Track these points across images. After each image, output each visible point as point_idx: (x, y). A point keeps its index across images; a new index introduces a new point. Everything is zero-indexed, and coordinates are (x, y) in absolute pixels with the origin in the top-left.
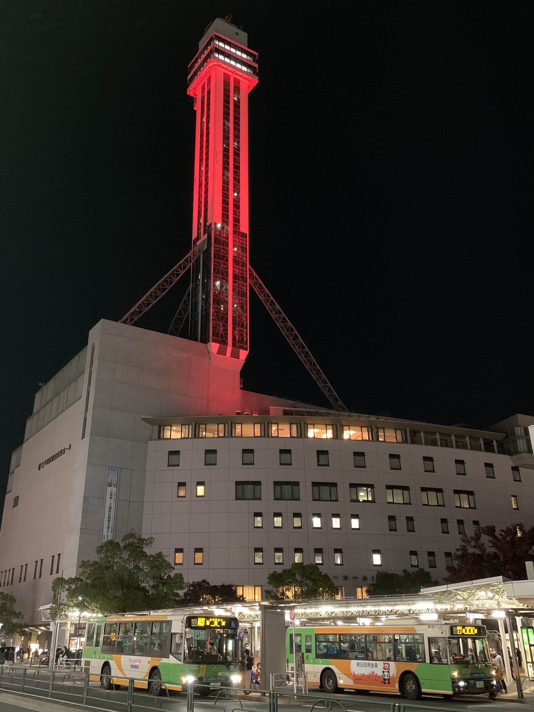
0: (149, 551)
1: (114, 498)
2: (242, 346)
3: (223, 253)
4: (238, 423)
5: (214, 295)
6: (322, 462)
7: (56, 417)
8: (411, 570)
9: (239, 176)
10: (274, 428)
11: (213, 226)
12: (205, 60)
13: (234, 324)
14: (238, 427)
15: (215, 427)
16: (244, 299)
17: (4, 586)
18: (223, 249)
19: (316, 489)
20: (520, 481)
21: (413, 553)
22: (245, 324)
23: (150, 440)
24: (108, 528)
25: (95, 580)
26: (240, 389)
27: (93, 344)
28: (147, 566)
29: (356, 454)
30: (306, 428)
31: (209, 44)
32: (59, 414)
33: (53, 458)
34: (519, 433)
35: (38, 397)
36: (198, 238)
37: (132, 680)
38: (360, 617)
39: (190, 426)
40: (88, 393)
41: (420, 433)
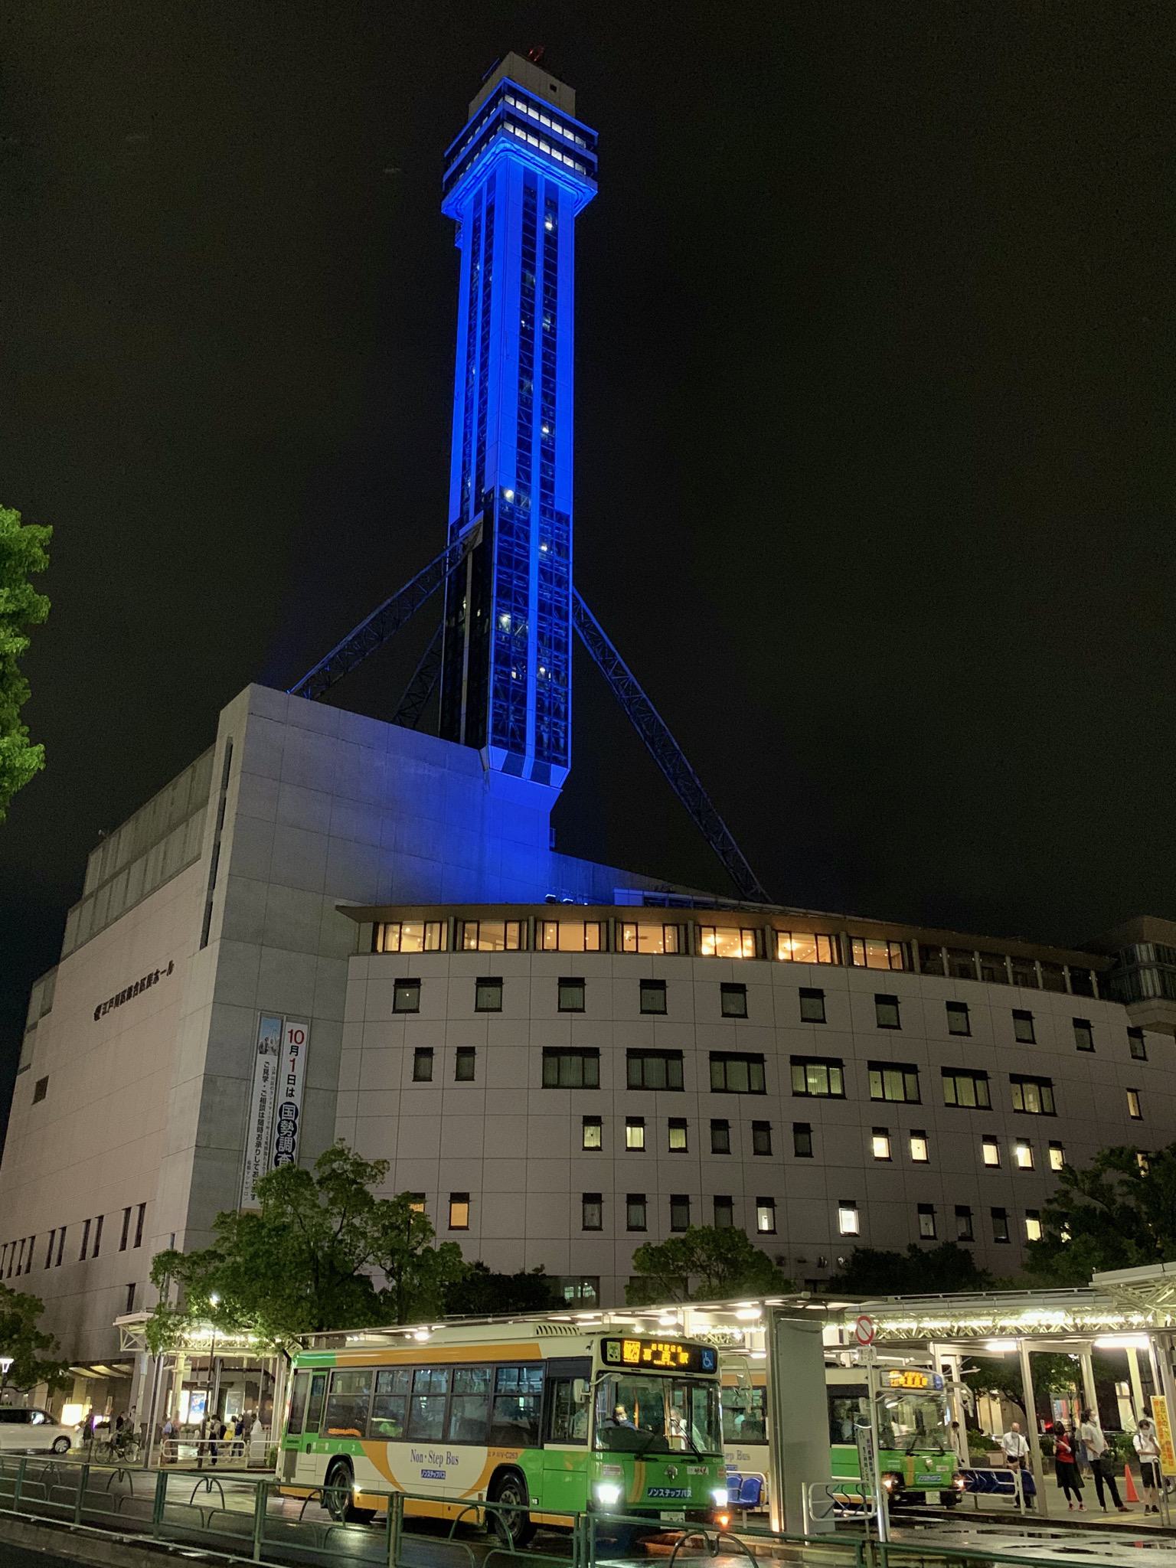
0: (381, 1191)
1: (273, 1078)
2: (555, 758)
3: (517, 554)
4: (550, 922)
5: (497, 645)
6: (732, 1009)
7: (137, 903)
8: (926, 1246)
9: (554, 390)
10: (628, 933)
11: (497, 495)
12: (484, 139)
13: (540, 709)
14: (551, 929)
15: (498, 928)
16: (562, 657)
17: (9, 1275)
18: (518, 545)
19: (719, 1066)
20: (1144, 1058)
21: (925, 1209)
22: (563, 710)
23: (353, 954)
24: (259, 1145)
25: (255, 1256)
26: (551, 849)
27: (230, 739)
28: (374, 1225)
29: (805, 993)
30: (698, 936)
31: (493, 103)
32: (143, 897)
33: (129, 993)
34: (1145, 959)
35: (95, 860)
36: (461, 522)
37: (163, 1474)
38: (938, 1340)
39: (445, 926)
40: (217, 847)
41: (939, 950)
